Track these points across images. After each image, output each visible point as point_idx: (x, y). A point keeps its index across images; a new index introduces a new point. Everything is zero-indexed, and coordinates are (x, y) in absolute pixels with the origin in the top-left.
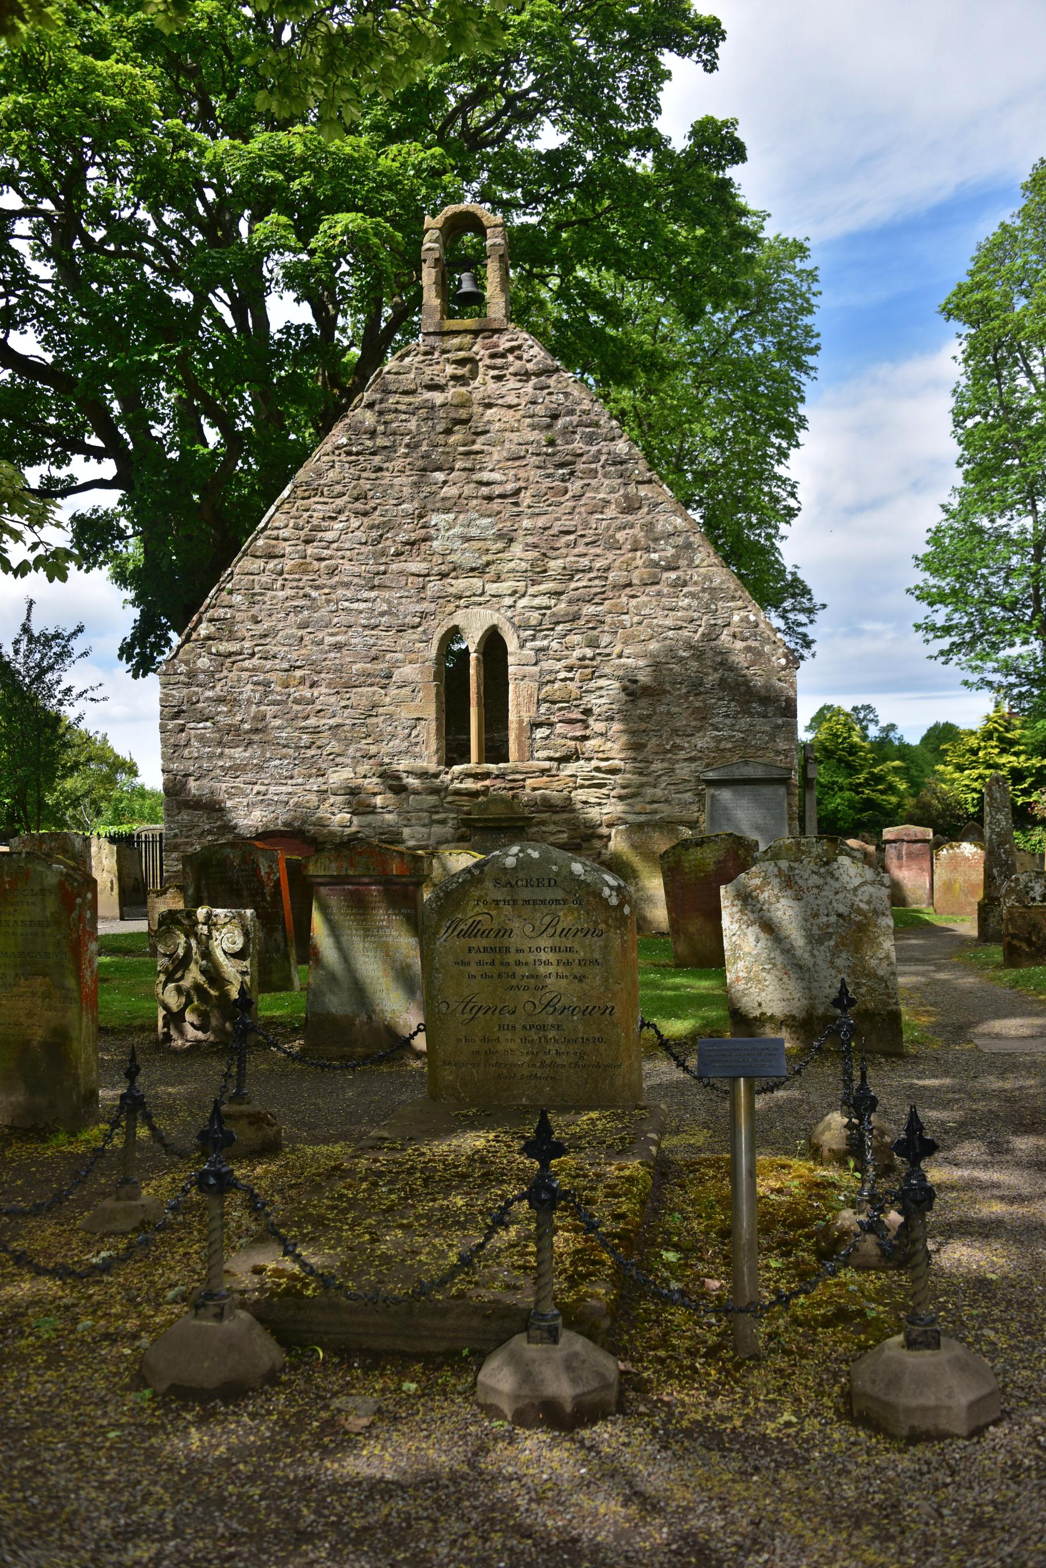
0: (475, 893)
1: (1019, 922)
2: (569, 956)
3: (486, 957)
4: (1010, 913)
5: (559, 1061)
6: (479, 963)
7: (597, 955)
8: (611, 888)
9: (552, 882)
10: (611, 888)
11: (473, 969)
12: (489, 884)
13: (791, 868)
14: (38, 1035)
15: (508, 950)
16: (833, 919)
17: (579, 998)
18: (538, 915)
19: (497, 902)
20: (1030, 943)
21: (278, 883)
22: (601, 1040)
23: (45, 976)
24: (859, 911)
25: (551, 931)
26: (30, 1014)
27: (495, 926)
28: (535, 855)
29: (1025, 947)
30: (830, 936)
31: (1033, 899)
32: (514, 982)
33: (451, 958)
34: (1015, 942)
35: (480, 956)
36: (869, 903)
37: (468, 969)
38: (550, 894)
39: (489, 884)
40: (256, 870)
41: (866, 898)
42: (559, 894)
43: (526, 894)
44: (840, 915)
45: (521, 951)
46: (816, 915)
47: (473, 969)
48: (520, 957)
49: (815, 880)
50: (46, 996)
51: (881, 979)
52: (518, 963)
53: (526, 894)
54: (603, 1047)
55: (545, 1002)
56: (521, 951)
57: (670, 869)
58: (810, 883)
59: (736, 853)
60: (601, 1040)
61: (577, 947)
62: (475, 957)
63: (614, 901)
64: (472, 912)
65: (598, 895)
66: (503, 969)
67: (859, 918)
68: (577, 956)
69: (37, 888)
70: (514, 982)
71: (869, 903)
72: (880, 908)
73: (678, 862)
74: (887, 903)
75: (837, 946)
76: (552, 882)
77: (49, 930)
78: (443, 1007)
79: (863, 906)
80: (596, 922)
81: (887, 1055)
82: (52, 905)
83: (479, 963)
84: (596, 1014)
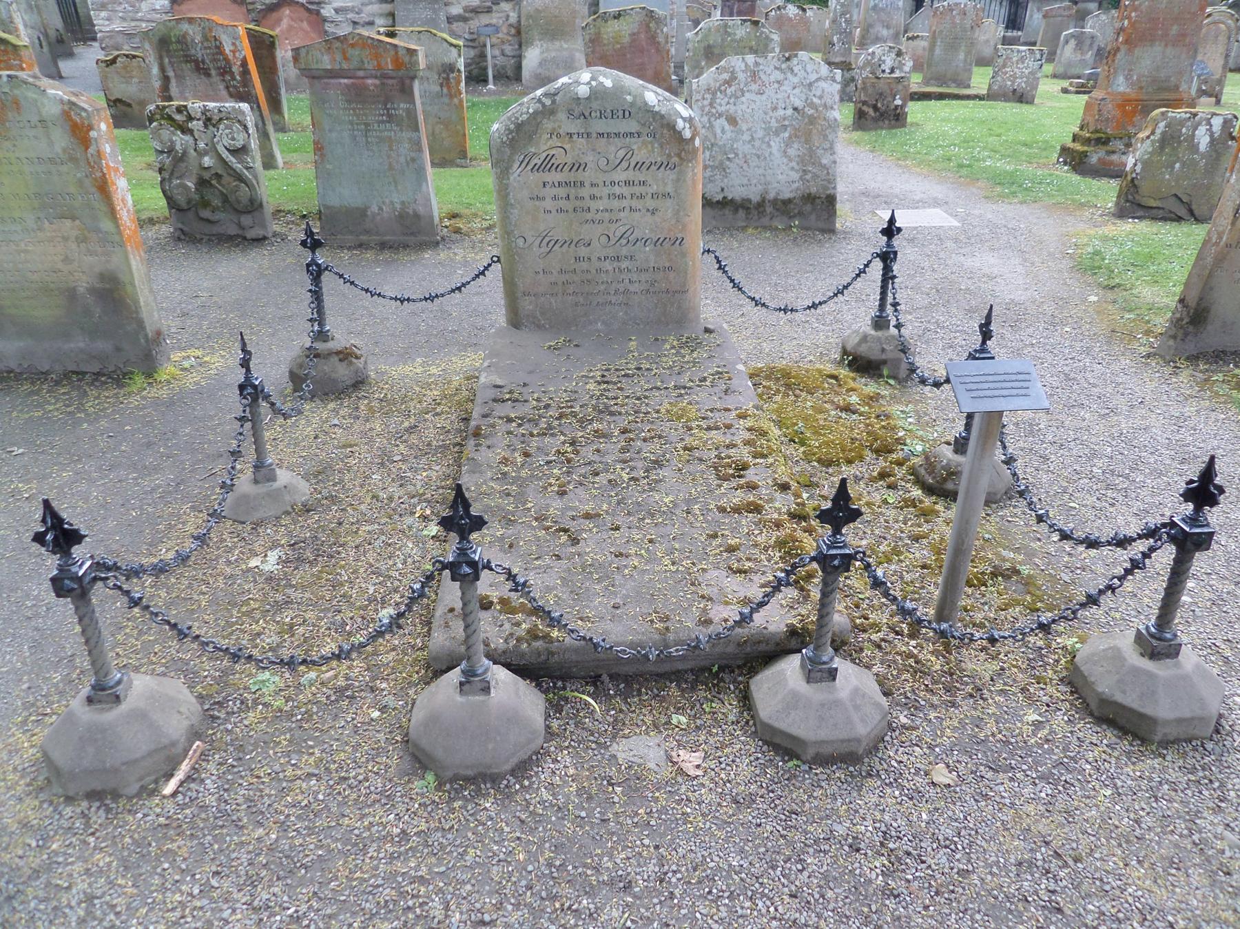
0: (548, 125)
1: (870, 91)
2: (641, 189)
3: (562, 192)
4: (864, 83)
5: (632, 289)
6: (555, 198)
7: (669, 189)
8: (684, 119)
9: (626, 114)
10: (684, 119)
11: (548, 204)
12: (562, 116)
13: (757, 64)
14: (83, 283)
15: (582, 184)
16: (790, 112)
17: (651, 230)
18: (613, 149)
19: (571, 135)
20: (875, 108)
21: (244, 63)
22: (670, 268)
23: (73, 218)
24: (812, 105)
25: (625, 164)
26: (67, 260)
27: (570, 161)
28: (608, 83)
29: (871, 112)
30: (785, 127)
31: (883, 71)
32: (589, 216)
33: (525, 193)
34: (865, 108)
35: (555, 191)
36: (821, 97)
37: (543, 204)
38: (632, 126)
39: (562, 116)
40: (219, 49)
41: (818, 93)
42: (632, 126)
43: (599, 126)
44: (795, 109)
45: (596, 185)
46: (775, 109)
47: (548, 204)
48: (595, 191)
49: (778, 75)
50: (82, 240)
51: (824, 167)
52: (593, 197)
53: (599, 126)
54: (672, 275)
55: (618, 234)
56: (596, 185)
57: (591, 41)
58: (772, 78)
59: (648, 26)
60: (670, 268)
61: (650, 181)
62: (550, 192)
63: (687, 134)
64: (543, 146)
65: (672, 127)
66: (578, 203)
67: (811, 112)
68: (650, 191)
69: (35, 119)
70: (589, 216)
71: (821, 97)
72: (829, 102)
73: (598, 34)
74: (837, 98)
75: (790, 137)
76: (626, 114)
77: (64, 168)
78: (520, 242)
79: (815, 100)
80: (669, 156)
81: (823, 231)
82: (61, 140)
83: (555, 198)
84: (667, 245)
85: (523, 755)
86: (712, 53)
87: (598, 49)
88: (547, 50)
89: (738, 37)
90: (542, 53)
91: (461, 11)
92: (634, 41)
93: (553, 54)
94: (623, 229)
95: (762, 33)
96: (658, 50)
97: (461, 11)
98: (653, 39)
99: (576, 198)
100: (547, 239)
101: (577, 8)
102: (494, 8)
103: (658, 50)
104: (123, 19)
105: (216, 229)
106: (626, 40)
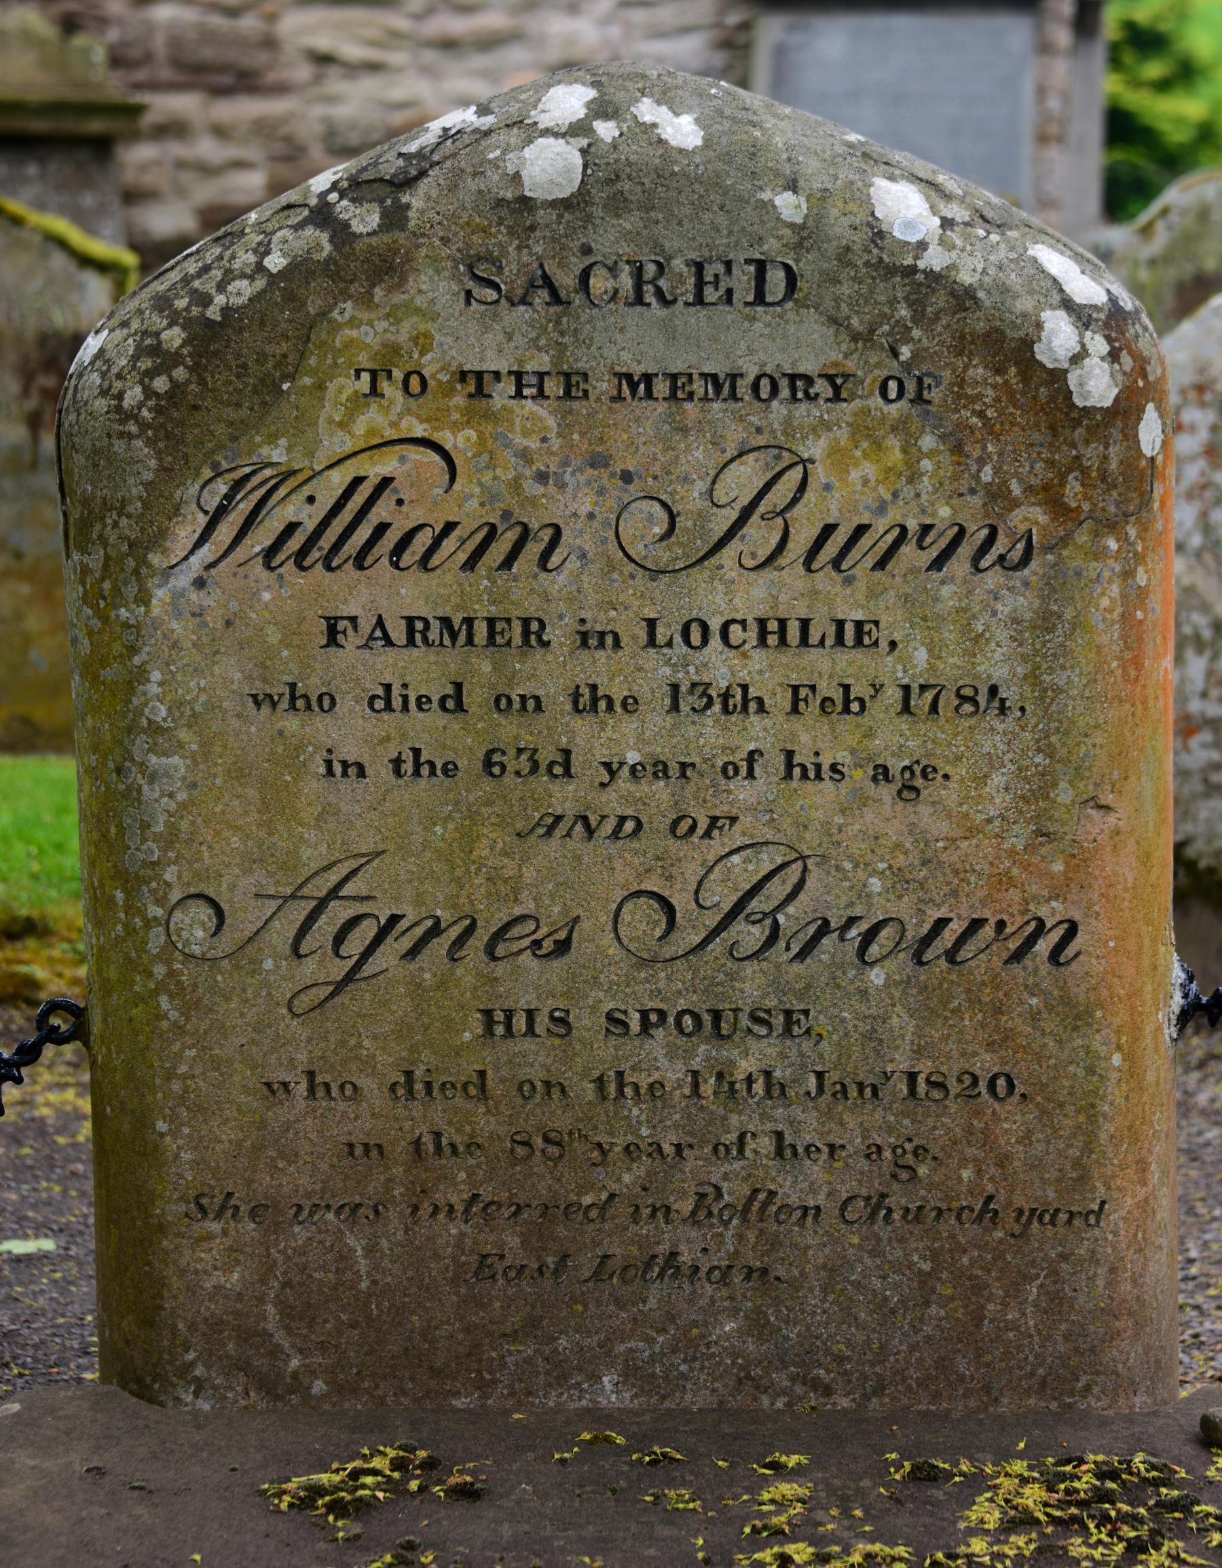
25: (760, 537)
62: (358, 667)
94: (744, 870)
99: (502, 703)
100: (339, 912)
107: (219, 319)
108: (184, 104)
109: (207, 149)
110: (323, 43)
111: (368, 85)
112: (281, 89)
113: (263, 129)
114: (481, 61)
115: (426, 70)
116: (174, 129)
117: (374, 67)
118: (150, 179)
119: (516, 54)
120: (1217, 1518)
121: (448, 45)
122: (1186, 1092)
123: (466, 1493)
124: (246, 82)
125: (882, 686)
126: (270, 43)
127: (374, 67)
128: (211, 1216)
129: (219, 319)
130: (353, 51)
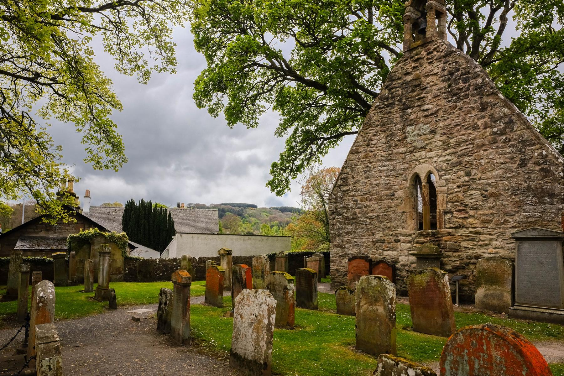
73: (413, 281)
85: (246, 237)
86: (364, 292)
87: (413, 288)
88: (489, 289)
89: (373, 285)
90: (486, 290)
91: (451, 268)
92: (428, 285)
93: (492, 292)
95: (383, 284)
96: (440, 292)
97: (451, 268)
98: (437, 285)
101: (506, 269)
102: (466, 267)
103: (440, 292)
104: (337, 266)
105: (430, 112)
106: (425, 284)
107: (138, 205)
108: (450, 253)
109: (453, 259)
110: (466, 246)
111: (471, 251)
112: (461, 251)
113: (459, 256)
114: (485, 247)
115: (478, 248)
116: (449, 256)
117: (472, 248)
118: (446, 262)
119: (490, 246)
120: (563, 164)
121: (481, 245)
122: (92, 160)
123: (87, 149)
124: (457, 251)
125: (203, 106)
126: (460, 246)
127: (472, 248)
128: (476, 21)
129: (138, 205)
130: (470, 246)
